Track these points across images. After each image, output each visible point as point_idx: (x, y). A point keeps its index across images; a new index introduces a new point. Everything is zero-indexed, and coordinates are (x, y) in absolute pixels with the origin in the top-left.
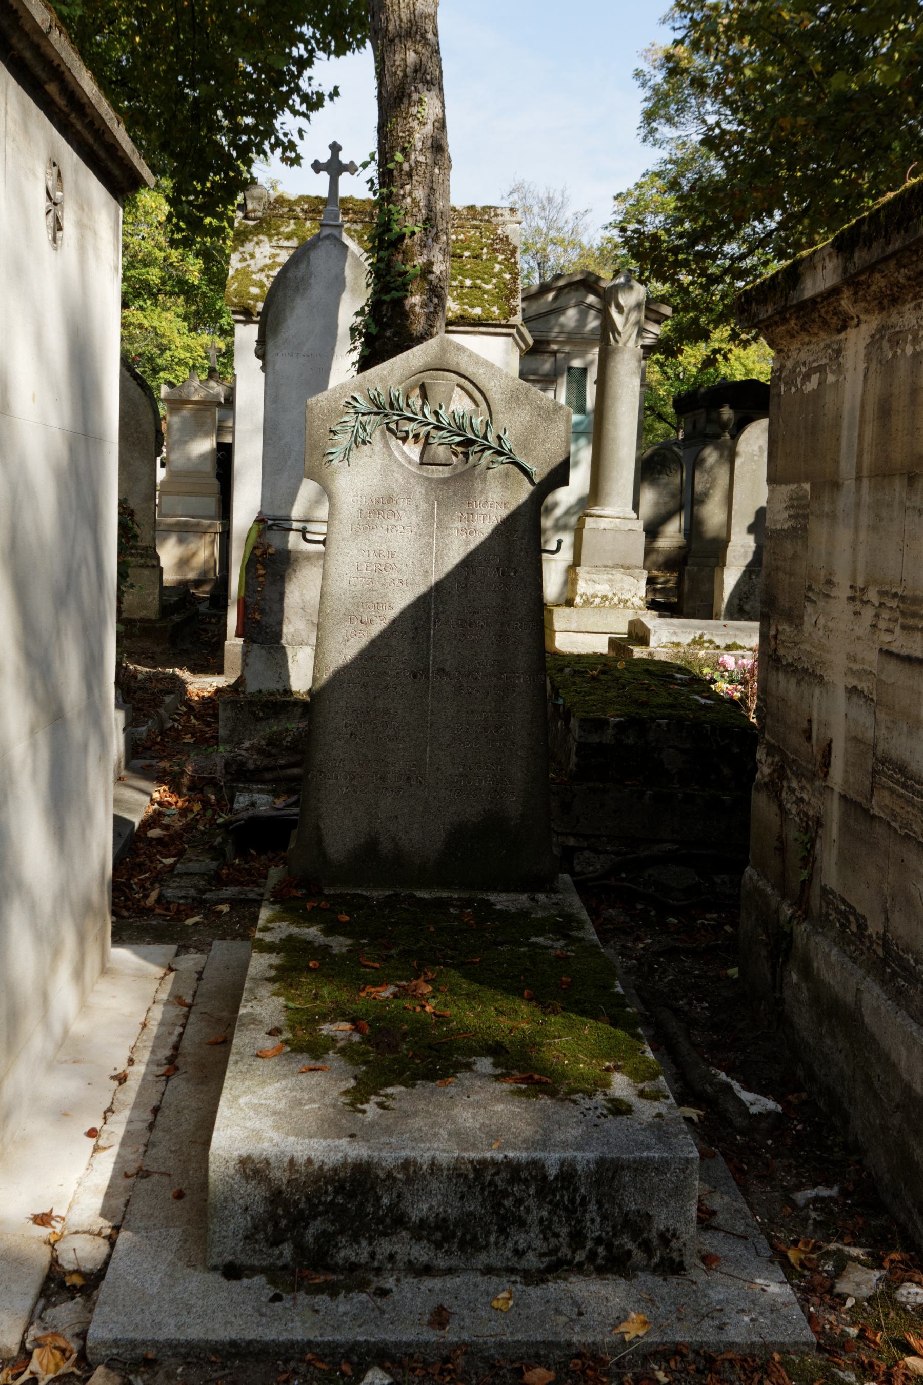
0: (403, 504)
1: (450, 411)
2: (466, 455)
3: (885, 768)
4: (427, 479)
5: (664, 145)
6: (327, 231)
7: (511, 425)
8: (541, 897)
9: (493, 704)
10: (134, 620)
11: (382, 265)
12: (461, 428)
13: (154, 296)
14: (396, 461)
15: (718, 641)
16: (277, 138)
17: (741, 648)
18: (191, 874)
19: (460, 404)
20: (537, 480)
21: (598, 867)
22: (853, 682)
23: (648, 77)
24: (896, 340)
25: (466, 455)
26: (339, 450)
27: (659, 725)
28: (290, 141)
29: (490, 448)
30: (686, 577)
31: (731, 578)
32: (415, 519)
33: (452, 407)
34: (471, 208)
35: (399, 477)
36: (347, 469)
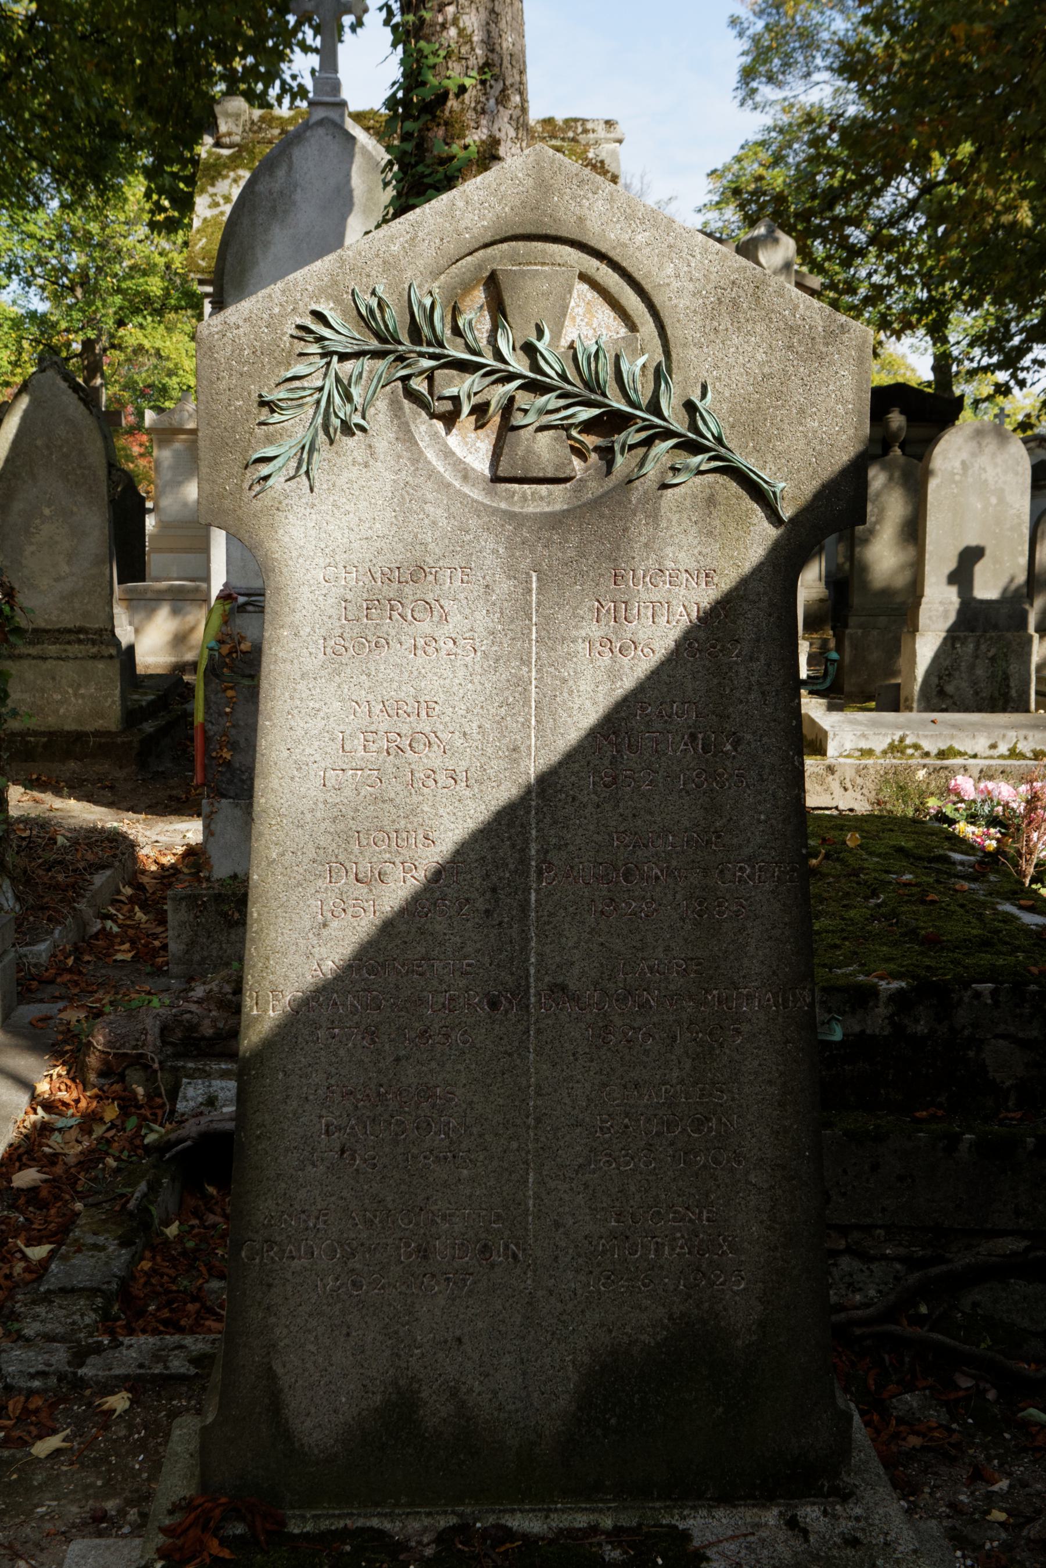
0: (451, 584)
1: (564, 343)
2: (607, 454)
4: (511, 516)
5: (767, 109)
6: (320, 113)
7: (721, 372)
8: (811, 1513)
9: (688, 1064)
10: (86, 734)
11: (409, 147)
12: (593, 384)
13: (159, 312)
14: (432, 474)
15: (927, 745)
16: (283, 83)
17: (961, 754)
18: (73, 1290)
19: (587, 324)
20: (787, 512)
21: (872, 1293)
23: (746, 25)
25: (607, 454)
26: (285, 450)
27: (978, 995)
28: (300, 86)
29: (668, 434)
30: (847, 643)
31: (926, 647)
32: (482, 620)
33: (570, 334)
34: (549, 121)
35: (438, 513)
36: (308, 497)
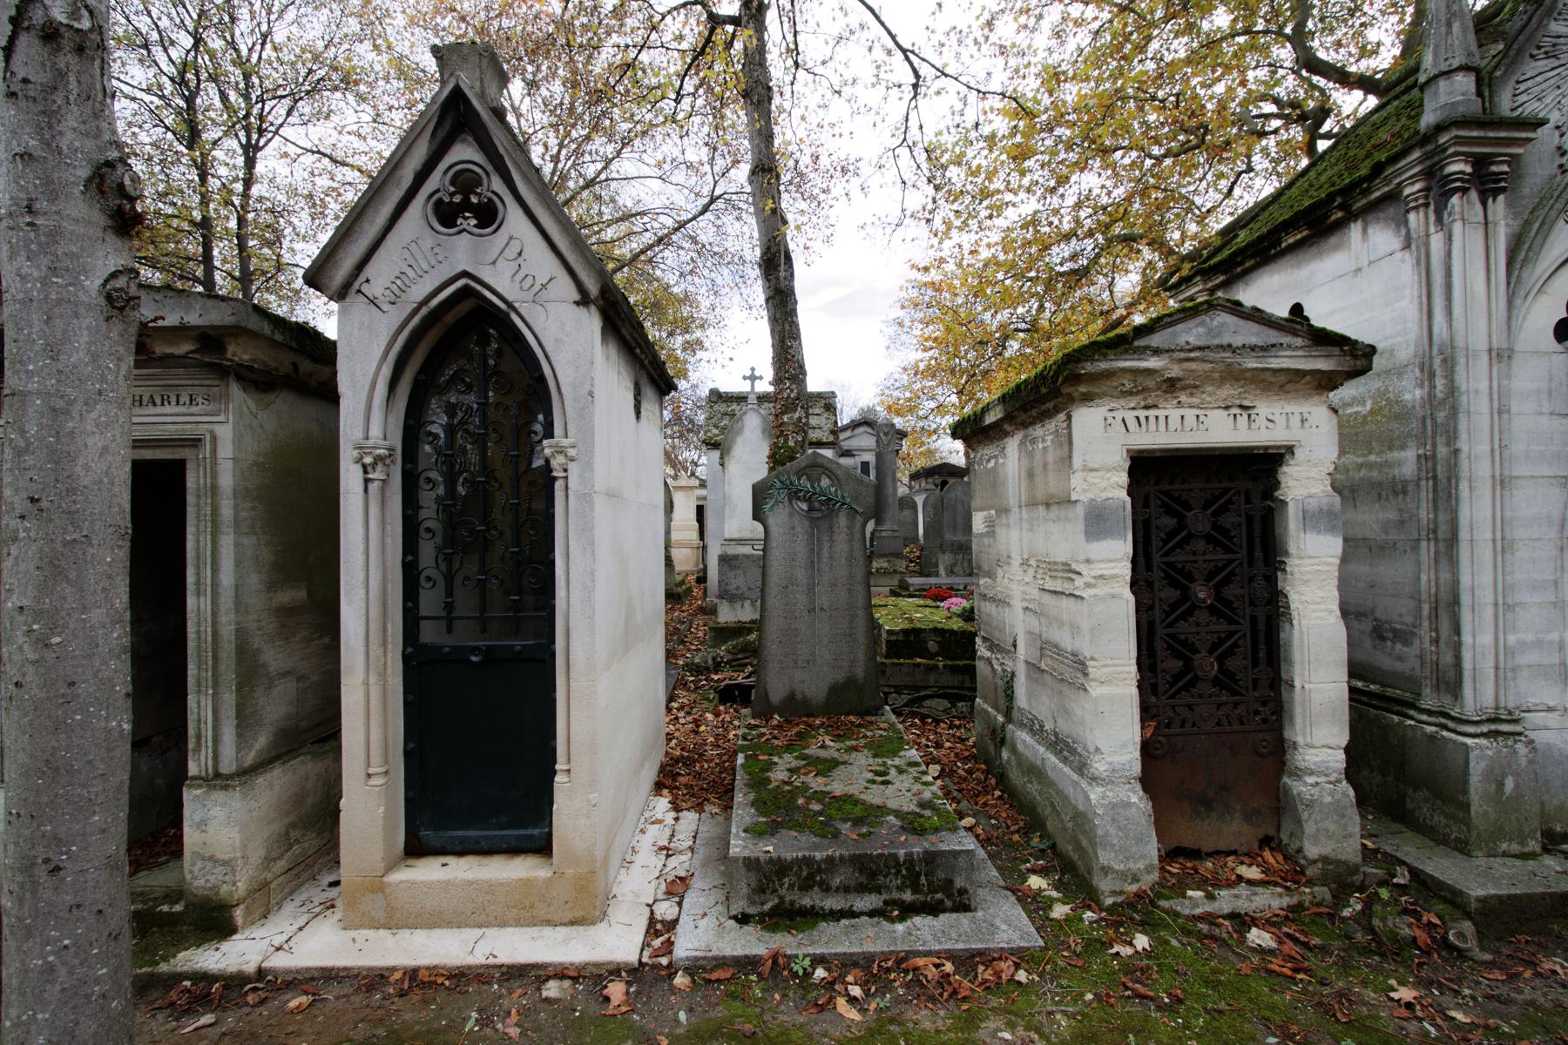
3: (1046, 647)
22: (1026, 604)
24: (1033, 442)
